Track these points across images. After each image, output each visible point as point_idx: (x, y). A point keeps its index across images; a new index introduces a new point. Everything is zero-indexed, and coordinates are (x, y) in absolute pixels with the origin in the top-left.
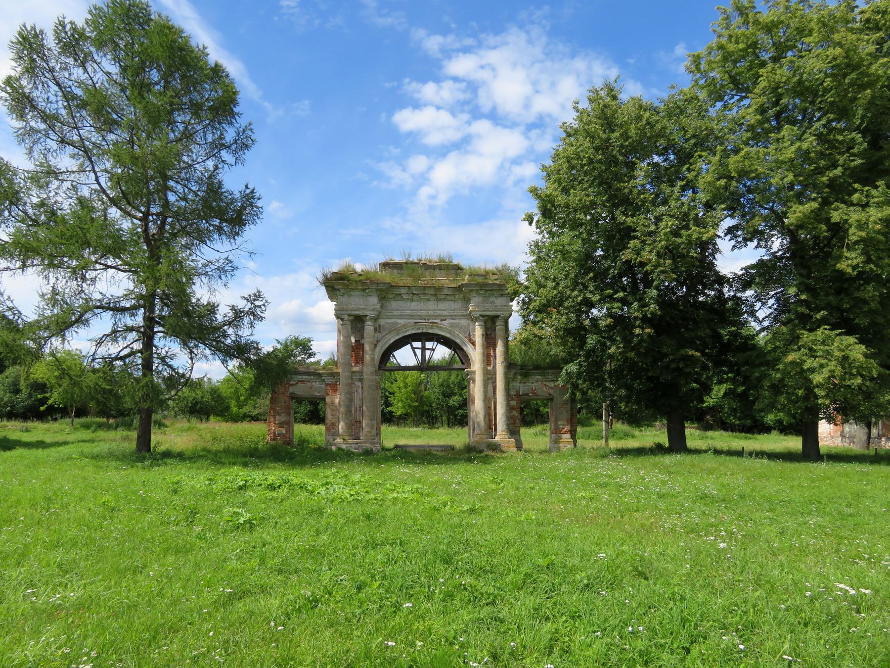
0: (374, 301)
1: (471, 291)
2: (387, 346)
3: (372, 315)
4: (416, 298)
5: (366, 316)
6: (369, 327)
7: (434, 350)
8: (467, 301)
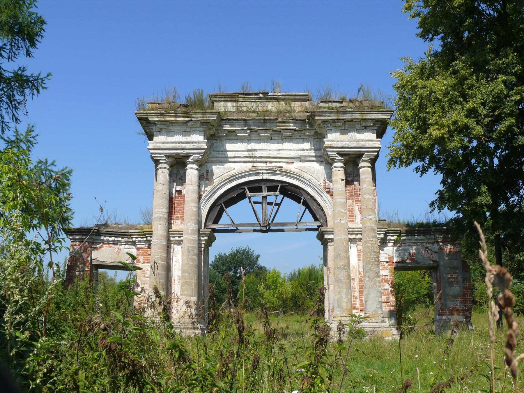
0: (197, 141)
1: (325, 121)
2: (216, 197)
3: (196, 155)
4: (254, 136)
5: (188, 157)
6: (192, 172)
7: (279, 205)
8: (318, 138)
